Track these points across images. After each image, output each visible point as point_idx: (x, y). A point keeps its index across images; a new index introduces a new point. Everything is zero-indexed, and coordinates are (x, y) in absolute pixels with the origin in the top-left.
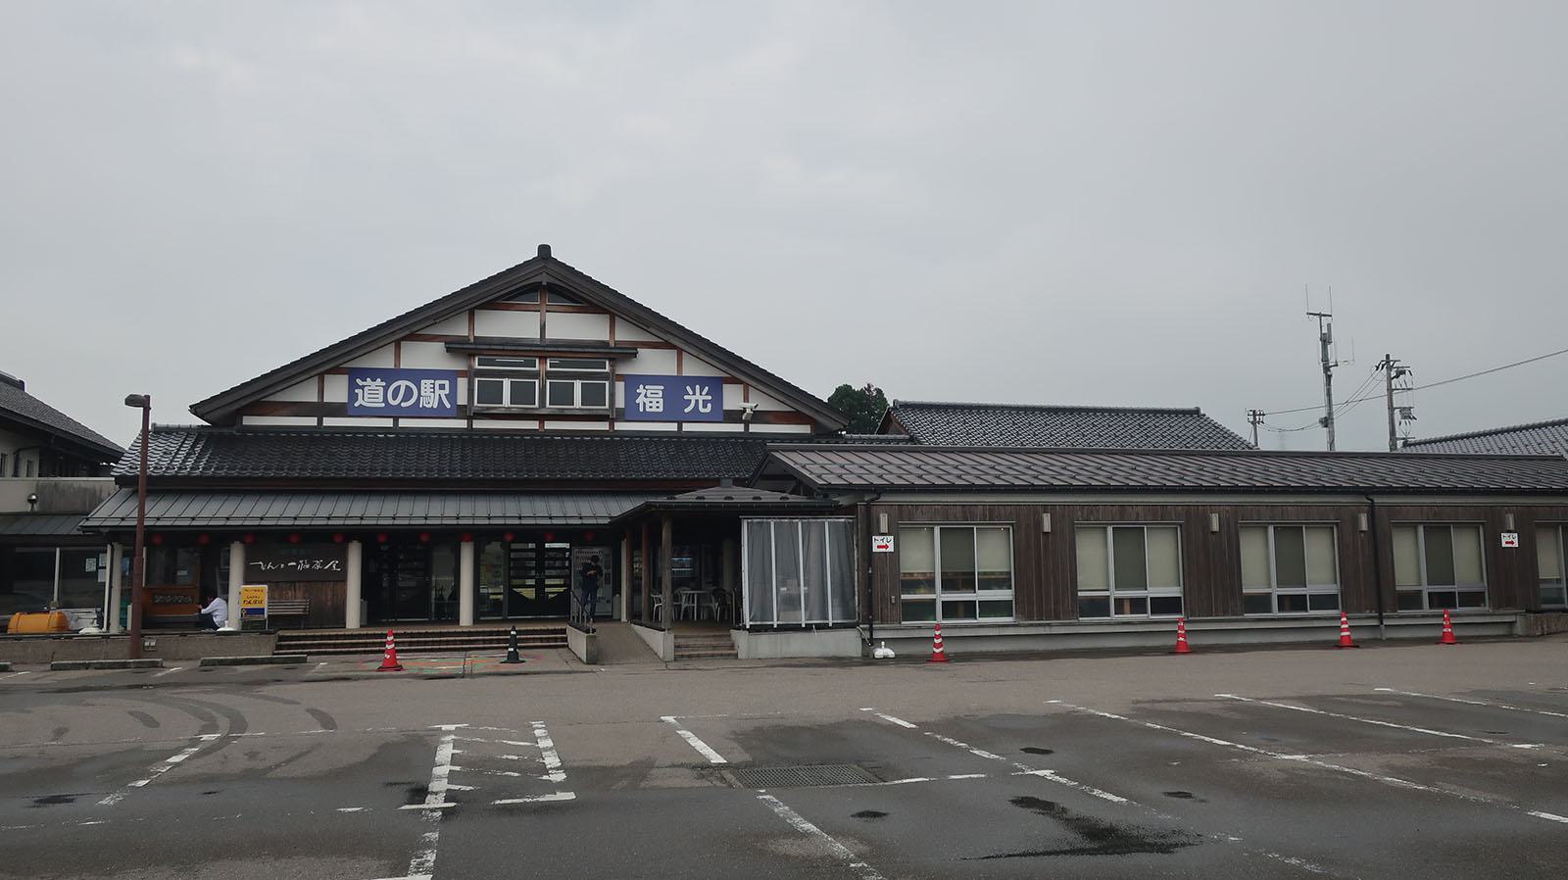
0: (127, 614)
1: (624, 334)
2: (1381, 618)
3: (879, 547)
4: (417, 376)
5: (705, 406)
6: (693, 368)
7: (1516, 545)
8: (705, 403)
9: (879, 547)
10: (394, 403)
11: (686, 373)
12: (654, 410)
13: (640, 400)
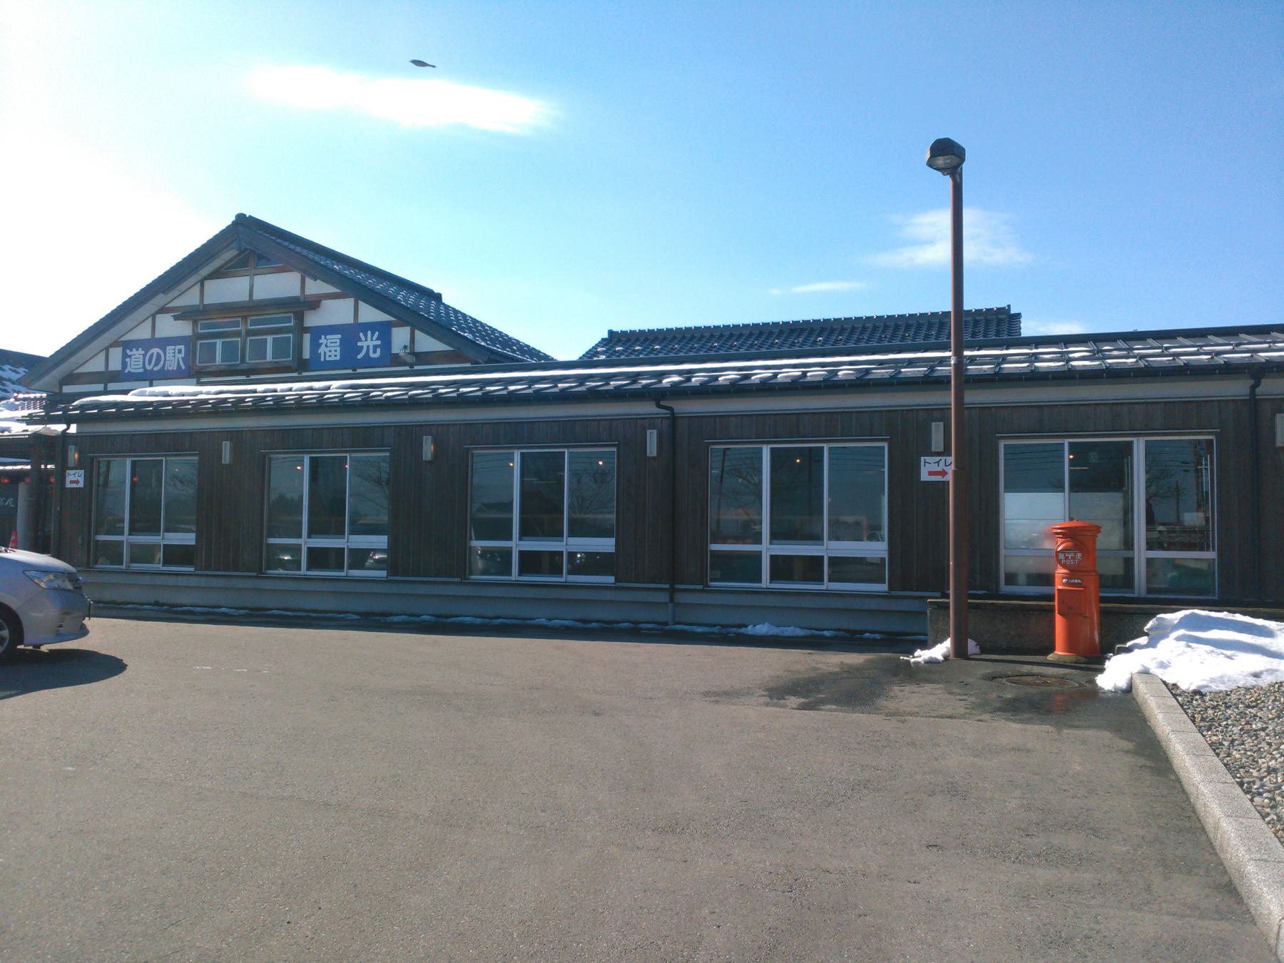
0: (761, 514)
1: (315, 287)
2: (673, 591)
3: (931, 473)
4: (164, 343)
5: (375, 352)
6: (370, 314)
7: (81, 485)
8: (375, 347)
9: (931, 473)
10: (149, 368)
11: (362, 320)
12: (333, 358)
13: (322, 350)
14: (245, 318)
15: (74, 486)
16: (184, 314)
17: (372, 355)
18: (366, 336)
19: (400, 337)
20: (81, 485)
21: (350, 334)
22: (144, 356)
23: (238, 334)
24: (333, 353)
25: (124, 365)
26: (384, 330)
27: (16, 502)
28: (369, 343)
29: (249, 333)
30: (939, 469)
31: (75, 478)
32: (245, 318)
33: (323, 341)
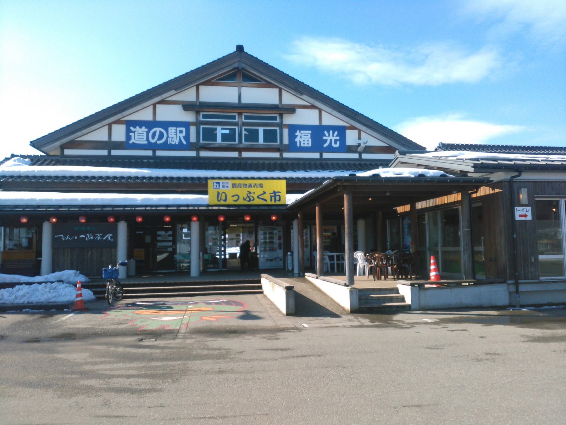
3: (520, 216)
4: (166, 125)
6: (330, 119)
7: (529, 218)
8: (336, 141)
9: (520, 216)
10: (153, 141)
11: (324, 123)
12: (306, 145)
14: (240, 114)
15: (523, 218)
16: (187, 106)
17: (334, 145)
18: (333, 133)
19: (351, 138)
20: (529, 218)
21: (318, 131)
22: (148, 133)
23: (236, 124)
24: (306, 142)
25: (128, 137)
26: (341, 131)
27: (115, 236)
28: (331, 138)
29: (244, 124)
30: (524, 214)
31: (523, 213)
32: (240, 114)
33: (298, 133)
